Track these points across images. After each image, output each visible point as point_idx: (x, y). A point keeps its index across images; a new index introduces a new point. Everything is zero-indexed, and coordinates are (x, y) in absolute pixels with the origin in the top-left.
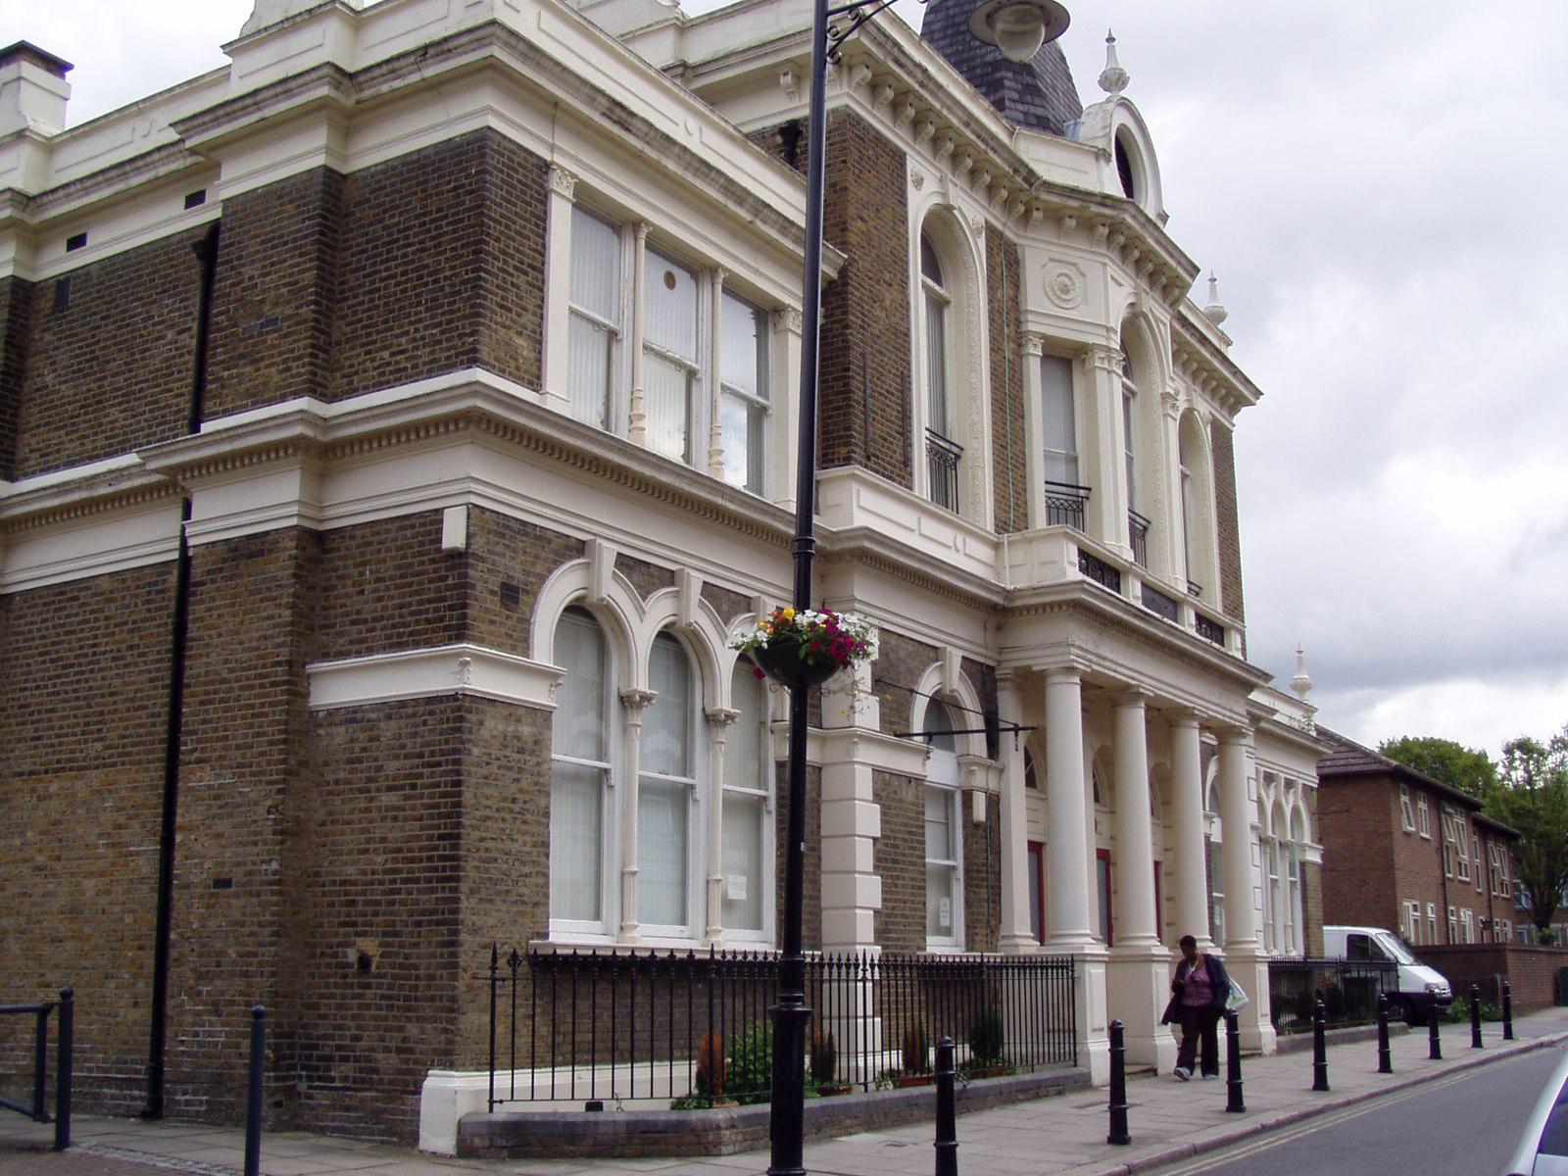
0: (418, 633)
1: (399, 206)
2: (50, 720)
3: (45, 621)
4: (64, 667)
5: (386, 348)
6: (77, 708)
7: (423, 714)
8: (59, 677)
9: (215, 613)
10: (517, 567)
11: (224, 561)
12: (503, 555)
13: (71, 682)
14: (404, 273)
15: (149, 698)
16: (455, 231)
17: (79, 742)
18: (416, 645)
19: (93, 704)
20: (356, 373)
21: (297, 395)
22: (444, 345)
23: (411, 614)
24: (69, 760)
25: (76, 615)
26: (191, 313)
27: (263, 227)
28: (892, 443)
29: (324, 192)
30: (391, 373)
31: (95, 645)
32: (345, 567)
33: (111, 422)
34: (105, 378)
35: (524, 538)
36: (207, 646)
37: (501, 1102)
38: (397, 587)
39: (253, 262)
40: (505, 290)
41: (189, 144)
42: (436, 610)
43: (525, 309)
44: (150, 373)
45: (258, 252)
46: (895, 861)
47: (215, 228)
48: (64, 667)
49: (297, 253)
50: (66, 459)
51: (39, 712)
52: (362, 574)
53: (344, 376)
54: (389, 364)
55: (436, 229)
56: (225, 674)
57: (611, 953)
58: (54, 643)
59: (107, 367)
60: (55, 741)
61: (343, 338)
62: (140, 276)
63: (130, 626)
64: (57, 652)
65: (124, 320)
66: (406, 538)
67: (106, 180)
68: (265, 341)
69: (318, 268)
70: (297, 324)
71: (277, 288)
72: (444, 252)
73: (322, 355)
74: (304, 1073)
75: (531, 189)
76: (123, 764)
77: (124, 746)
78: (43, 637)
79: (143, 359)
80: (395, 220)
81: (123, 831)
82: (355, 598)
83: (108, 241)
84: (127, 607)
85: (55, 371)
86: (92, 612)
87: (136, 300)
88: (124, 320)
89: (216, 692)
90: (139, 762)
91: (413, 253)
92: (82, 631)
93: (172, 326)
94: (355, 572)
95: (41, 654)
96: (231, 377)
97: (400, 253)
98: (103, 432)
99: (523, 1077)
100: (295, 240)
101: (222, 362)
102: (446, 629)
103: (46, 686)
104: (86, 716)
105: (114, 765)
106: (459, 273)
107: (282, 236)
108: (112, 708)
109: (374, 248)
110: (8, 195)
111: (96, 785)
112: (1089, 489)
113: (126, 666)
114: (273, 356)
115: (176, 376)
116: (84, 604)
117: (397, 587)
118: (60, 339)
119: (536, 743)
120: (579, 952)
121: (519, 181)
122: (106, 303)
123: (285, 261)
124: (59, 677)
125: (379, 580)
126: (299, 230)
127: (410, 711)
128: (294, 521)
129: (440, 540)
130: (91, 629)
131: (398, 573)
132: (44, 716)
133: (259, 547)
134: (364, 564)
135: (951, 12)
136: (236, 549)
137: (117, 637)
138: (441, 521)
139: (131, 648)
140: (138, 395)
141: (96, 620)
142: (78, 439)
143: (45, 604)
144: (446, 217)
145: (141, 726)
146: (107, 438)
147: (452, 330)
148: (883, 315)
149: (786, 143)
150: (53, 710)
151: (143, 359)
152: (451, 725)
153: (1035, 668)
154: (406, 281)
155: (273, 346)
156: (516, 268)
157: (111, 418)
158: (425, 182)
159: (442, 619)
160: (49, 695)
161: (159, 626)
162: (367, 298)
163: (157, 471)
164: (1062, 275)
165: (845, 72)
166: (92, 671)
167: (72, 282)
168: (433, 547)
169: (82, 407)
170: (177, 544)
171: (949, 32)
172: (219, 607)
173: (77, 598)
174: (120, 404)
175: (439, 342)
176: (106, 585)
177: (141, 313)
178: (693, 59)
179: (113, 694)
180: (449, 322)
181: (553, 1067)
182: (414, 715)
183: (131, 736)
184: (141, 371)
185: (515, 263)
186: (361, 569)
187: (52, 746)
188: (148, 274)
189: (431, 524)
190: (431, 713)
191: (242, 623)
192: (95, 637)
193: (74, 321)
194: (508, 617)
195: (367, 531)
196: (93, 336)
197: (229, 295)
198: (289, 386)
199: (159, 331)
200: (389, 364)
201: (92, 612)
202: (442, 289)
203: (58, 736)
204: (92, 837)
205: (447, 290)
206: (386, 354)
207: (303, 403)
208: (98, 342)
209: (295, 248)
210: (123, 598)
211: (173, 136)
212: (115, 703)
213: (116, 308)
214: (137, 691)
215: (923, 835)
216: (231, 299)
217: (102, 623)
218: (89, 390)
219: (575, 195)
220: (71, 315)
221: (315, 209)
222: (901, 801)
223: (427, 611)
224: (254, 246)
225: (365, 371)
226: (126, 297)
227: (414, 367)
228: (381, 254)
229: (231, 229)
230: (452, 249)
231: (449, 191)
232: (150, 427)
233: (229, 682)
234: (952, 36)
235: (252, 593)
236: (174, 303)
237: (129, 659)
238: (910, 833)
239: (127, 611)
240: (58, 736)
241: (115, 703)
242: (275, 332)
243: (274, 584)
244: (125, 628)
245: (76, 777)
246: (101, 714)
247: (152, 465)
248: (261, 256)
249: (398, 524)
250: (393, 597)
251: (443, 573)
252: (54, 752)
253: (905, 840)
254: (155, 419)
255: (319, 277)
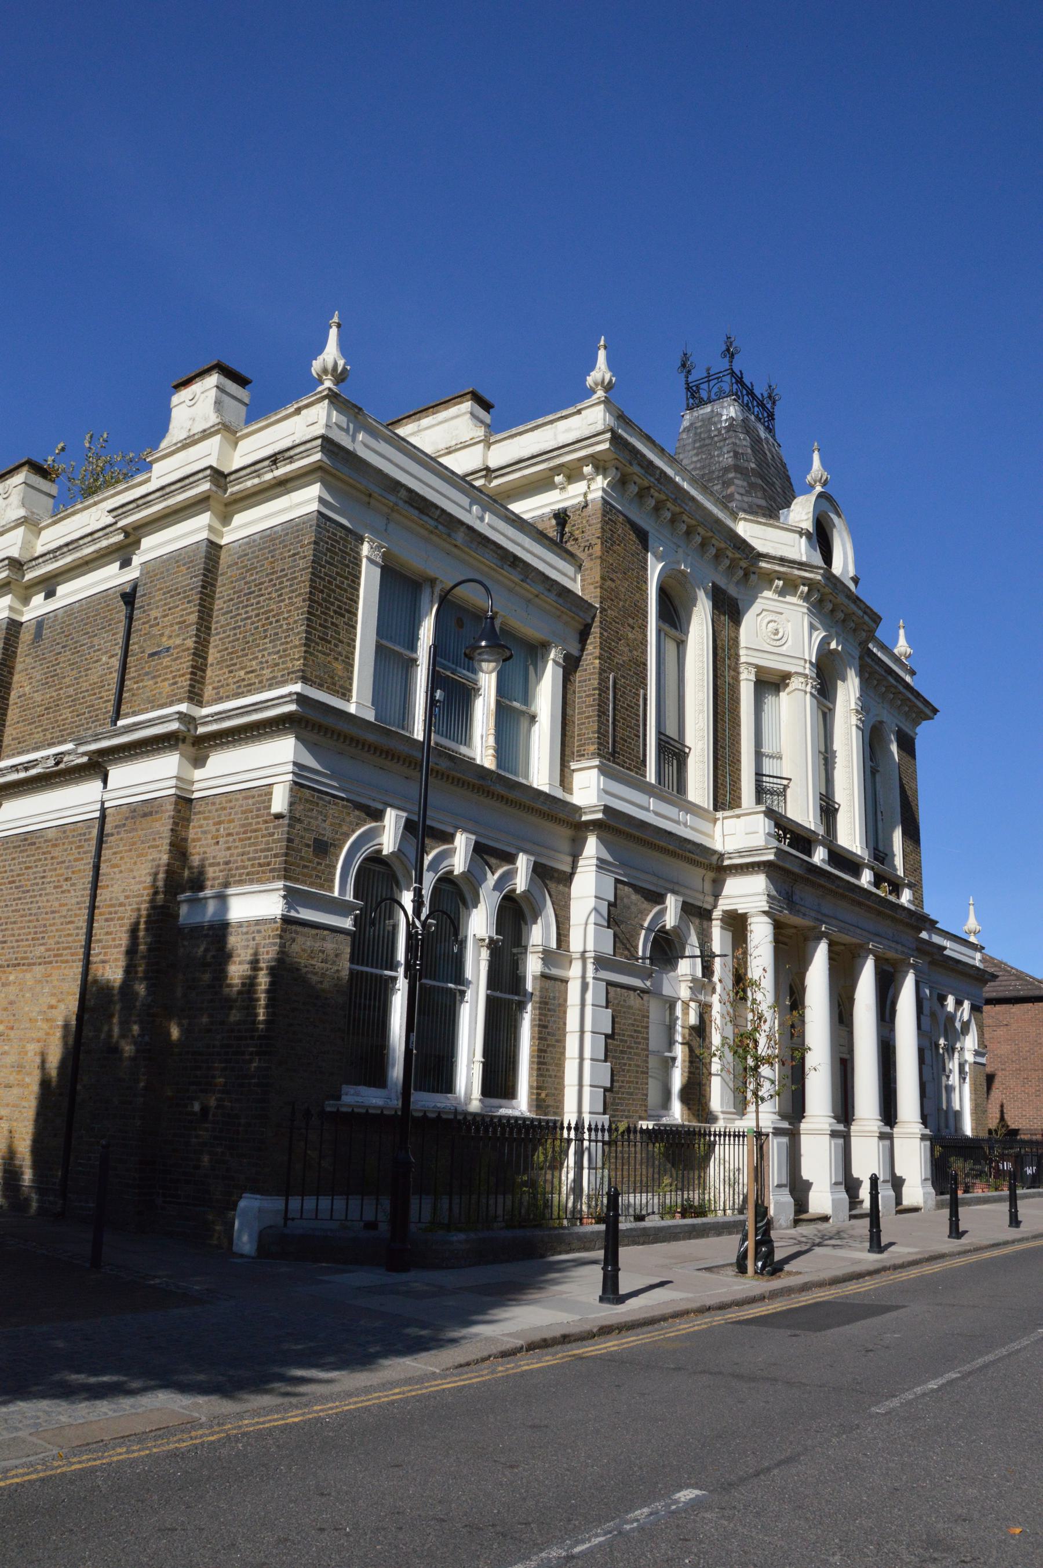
0: (253, 873)
1: (256, 568)
2: (13, 929)
3: (13, 859)
4: (24, 892)
5: (242, 668)
6: (30, 921)
7: (253, 932)
8: (20, 899)
9: (119, 856)
10: (328, 827)
11: (127, 819)
12: (316, 819)
13: (27, 903)
14: (258, 615)
15: (76, 915)
16: (291, 585)
17: (29, 946)
18: (251, 882)
19: (40, 919)
20: (222, 686)
21: (180, 701)
22: (281, 666)
23: (249, 859)
24: (23, 958)
25: (33, 855)
26: (118, 644)
27: (165, 582)
28: (630, 743)
29: (206, 557)
30: (245, 686)
31: (43, 877)
32: (208, 825)
33: (63, 720)
34: (61, 689)
35: (334, 807)
36: (112, 879)
37: (293, 1219)
38: (241, 840)
39: (157, 607)
40: (325, 627)
41: (120, 524)
42: (266, 857)
43: (341, 642)
44: (90, 685)
45: (161, 600)
46: (622, 1052)
47: (135, 585)
48: (24, 892)
49: (186, 600)
50: (34, 746)
51: (6, 924)
52: (218, 830)
53: (214, 688)
54: (244, 680)
55: (280, 584)
56: (122, 899)
57: (393, 1113)
58: (19, 875)
59: (64, 681)
60: (15, 944)
61: (215, 662)
62: (88, 618)
63: (67, 864)
64: (20, 881)
65: (76, 648)
66: (248, 805)
67: (69, 551)
68: (162, 663)
69: (199, 611)
70: (184, 651)
71: (172, 625)
72: (284, 600)
73: (199, 673)
74: (161, 1191)
75: (350, 555)
76: (57, 962)
77: (58, 949)
78: (12, 871)
79: (86, 676)
80: (253, 578)
81: (53, 1011)
82: (213, 847)
83: (70, 592)
84: (66, 850)
85: (31, 683)
86: (44, 853)
87: (85, 634)
88: (76, 648)
89: (116, 913)
90: (67, 962)
91: (264, 601)
92: (36, 866)
93: (106, 652)
94: (213, 828)
95: (10, 883)
96: (138, 688)
97: (255, 601)
98: (58, 726)
99: (310, 1203)
100: (185, 592)
101: (134, 678)
102: (272, 871)
103: (12, 905)
104: (35, 927)
105: (51, 962)
106: (293, 615)
107: (177, 589)
108: (52, 922)
109: (239, 597)
110: (6, 562)
111: (39, 976)
112: (790, 779)
113: (62, 892)
114: (166, 674)
115: (106, 687)
116: (39, 848)
117: (241, 840)
118: (36, 661)
119: (337, 956)
120: (356, 1110)
121: (340, 550)
122: (66, 636)
123: (177, 607)
124: (20, 899)
125: (229, 835)
126: (188, 585)
127: (244, 930)
128: (173, 791)
129: (269, 807)
130: (42, 866)
131: (242, 830)
132: (10, 926)
133: (149, 809)
134: (220, 823)
135: (699, 431)
136: (135, 811)
137: (58, 872)
138: (271, 794)
139: (66, 880)
140: (82, 701)
141: (46, 859)
142: (42, 731)
143: (14, 847)
144: (286, 575)
145: (69, 935)
146: (60, 731)
147: (286, 656)
148: (626, 649)
149: (558, 524)
150: (15, 923)
151: (86, 676)
152: (271, 941)
153: (740, 911)
154: (258, 621)
155: (167, 667)
156: (335, 612)
157: (64, 717)
158: (275, 550)
159: (269, 864)
160: (13, 911)
161: (85, 864)
162: (232, 633)
163: (84, 754)
164: (769, 623)
165: (601, 470)
166: (41, 895)
167: (46, 622)
168: (266, 812)
169: (46, 709)
170: (98, 806)
171: (697, 445)
172: (121, 852)
173: (35, 843)
174: (70, 707)
175: (277, 665)
176: (50, 834)
177: (87, 644)
178: (493, 464)
179: (53, 912)
180: (284, 651)
181: (333, 1195)
182: (247, 933)
183: (63, 943)
184: (85, 684)
185: (335, 608)
186: (217, 827)
187: (13, 947)
188: (93, 617)
189: (266, 795)
190: (259, 932)
191: (135, 863)
192: (45, 871)
193: (45, 649)
194: (319, 864)
195: (224, 799)
196: (56, 659)
197: (141, 630)
198: (174, 695)
199: (97, 656)
200: (244, 680)
201: (44, 853)
202: (281, 626)
203: (17, 941)
204: (34, 1014)
205: (285, 627)
206: (242, 673)
207: (183, 707)
208: (58, 664)
209: (185, 598)
210: (64, 844)
211: (110, 520)
212: (54, 918)
213: (72, 639)
214: (68, 910)
215: (647, 1033)
216: (142, 633)
217: (49, 862)
218: (51, 697)
219: (383, 560)
220: (44, 644)
221: (199, 570)
222: (630, 1007)
223: (259, 858)
224: (158, 596)
225: (228, 685)
226: (78, 632)
227: (260, 682)
228: (242, 602)
229: (145, 584)
230: (290, 598)
231: (289, 557)
232: (88, 723)
233: (125, 906)
234: (698, 448)
235: (143, 842)
236: (108, 636)
237: (65, 888)
238: (635, 1031)
239: (65, 853)
240: (17, 941)
241: (54, 918)
242: (168, 656)
243: (157, 836)
244: (63, 865)
245: (26, 971)
246: (45, 926)
247: (83, 749)
248: (163, 603)
249: (244, 794)
250: (237, 847)
251: (272, 830)
252: (14, 952)
253: (632, 1036)
254: (91, 717)
255: (200, 618)
